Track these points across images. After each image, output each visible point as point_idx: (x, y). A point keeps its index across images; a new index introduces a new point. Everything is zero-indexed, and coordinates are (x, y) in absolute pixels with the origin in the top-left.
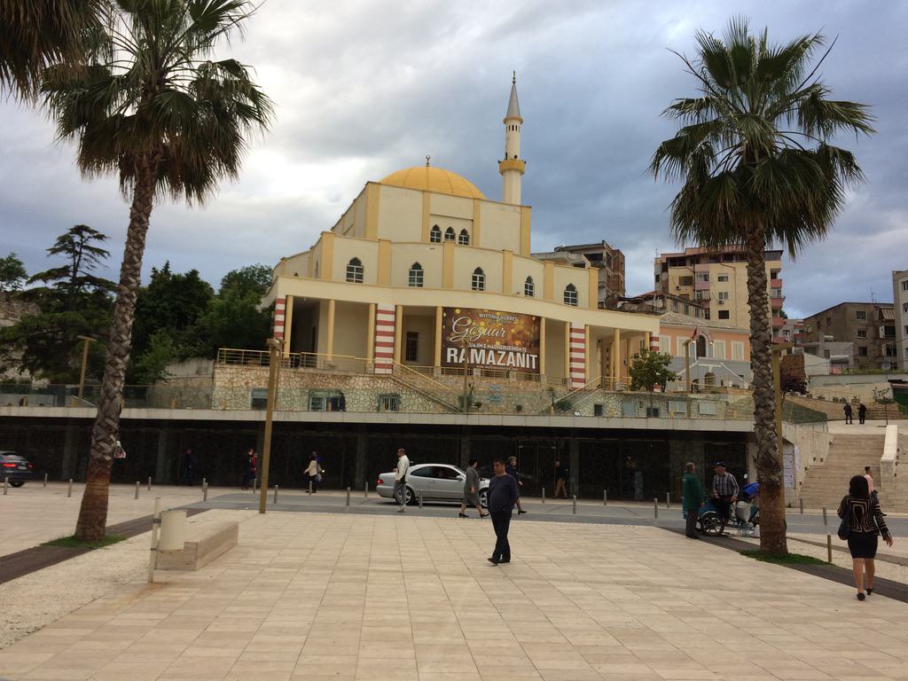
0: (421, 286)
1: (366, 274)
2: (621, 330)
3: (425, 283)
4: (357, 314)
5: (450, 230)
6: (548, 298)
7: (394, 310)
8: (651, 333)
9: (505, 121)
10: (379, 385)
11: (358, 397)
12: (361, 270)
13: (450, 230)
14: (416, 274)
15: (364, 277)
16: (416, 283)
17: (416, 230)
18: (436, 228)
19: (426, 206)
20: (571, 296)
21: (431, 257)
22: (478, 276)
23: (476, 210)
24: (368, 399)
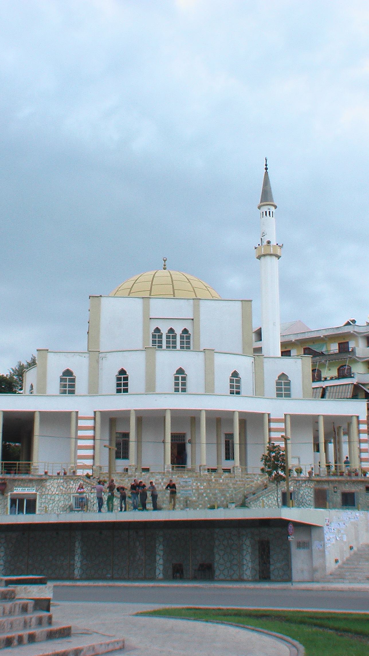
0: (126, 391)
2: (207, 411)
3: (130, 387)
4: (62, 420)
5: (171, 331)
6: (259, 392)
7: (93, 416)
8: (269, 414)
9: (259, 208)
10: (71, 486)
11: (53, 497)
12: (73, 380)
13: (171, 331)
15: (115, 385)
18: (157, 330)
19: (146, 309)
20: (283, 386)
22: (180, 376)
23: (196, 309)
24: (62, 498)
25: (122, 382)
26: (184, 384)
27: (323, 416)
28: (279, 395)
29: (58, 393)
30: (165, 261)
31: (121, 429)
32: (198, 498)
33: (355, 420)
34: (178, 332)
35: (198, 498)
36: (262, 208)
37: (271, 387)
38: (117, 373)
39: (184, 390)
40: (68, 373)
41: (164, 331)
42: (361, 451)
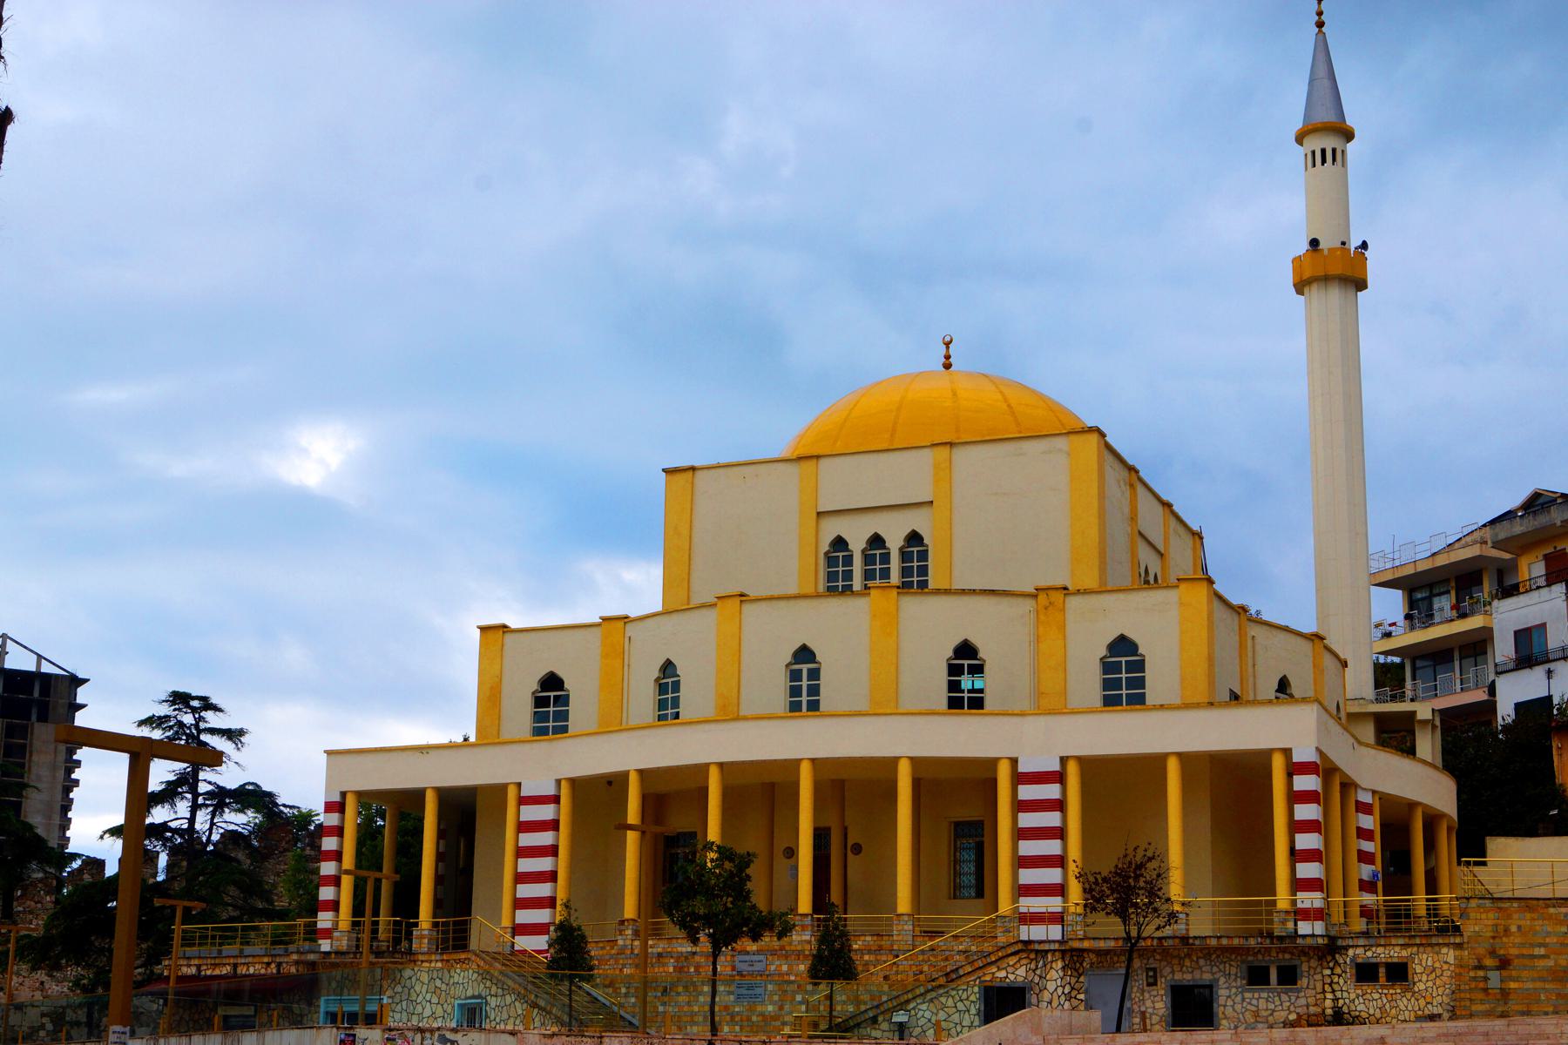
1: (574, 708)
4: (961, 806)
5: (876, 541)
8: (1287, 752)
9: (1300, 139)
12: (1139, 666)
13: (876, 541)
14: (804, 680)
15: (945, 686)
16: (966, 695)
17: (796, 563)
18: (840, 543)
21: (843, 630)
22: (805, 668)
25: (1123, 673)
26: (814, 690)
27: (1179, 755)
28: (1110, 702)
29: (943, 704)
30: (947, 344)
31: (679, 823)
32: (781, 1008)
33: (1278, 764)
34: (894, 543)
35: (781, 1008)
36: (1305, 141)
37: (1088, 682)
38: (535, 686)
39: (814, 706)
40: (1123, 645)
41: (857, 545)
42: (1296, 856)
